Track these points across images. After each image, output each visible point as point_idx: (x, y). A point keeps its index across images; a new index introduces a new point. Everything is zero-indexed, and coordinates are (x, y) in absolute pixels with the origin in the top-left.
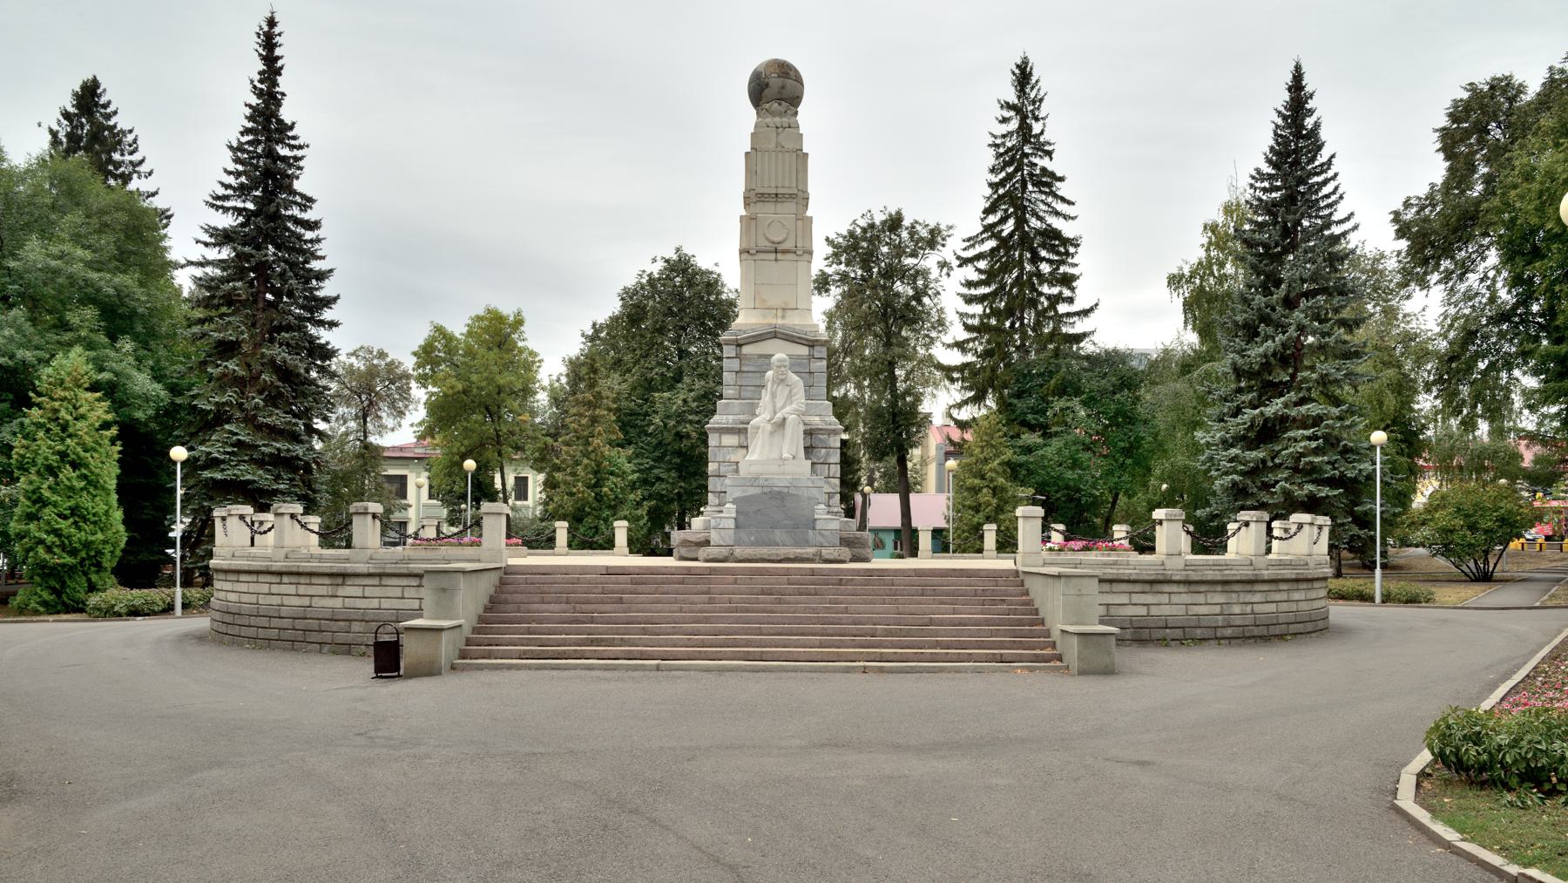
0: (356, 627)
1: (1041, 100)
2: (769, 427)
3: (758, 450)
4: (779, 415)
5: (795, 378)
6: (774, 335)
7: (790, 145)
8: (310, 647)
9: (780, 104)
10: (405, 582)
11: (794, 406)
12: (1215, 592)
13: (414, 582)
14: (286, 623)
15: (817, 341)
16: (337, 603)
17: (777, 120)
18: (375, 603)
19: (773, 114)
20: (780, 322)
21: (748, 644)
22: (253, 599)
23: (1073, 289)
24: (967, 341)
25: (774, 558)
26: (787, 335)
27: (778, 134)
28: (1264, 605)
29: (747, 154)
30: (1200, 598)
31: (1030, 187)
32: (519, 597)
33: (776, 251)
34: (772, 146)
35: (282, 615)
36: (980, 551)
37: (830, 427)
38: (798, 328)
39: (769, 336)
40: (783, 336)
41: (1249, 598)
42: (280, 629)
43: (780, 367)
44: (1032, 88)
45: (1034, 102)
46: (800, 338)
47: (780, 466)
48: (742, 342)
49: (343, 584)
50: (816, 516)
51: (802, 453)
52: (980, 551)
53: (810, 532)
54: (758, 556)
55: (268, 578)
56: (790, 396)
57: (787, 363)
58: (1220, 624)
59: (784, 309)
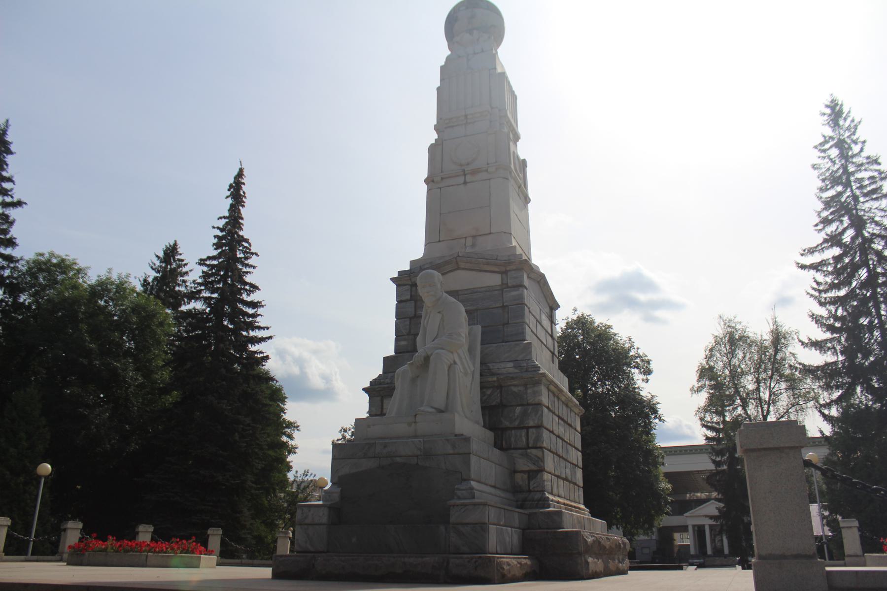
1: (856, 127)
23: (820, 180)
24: (826, 341)
31: (862, 199)
44: (845, 119)
45: (848, 129)
47: (409, 424)
53: (442, 528)
59: (474, 237)
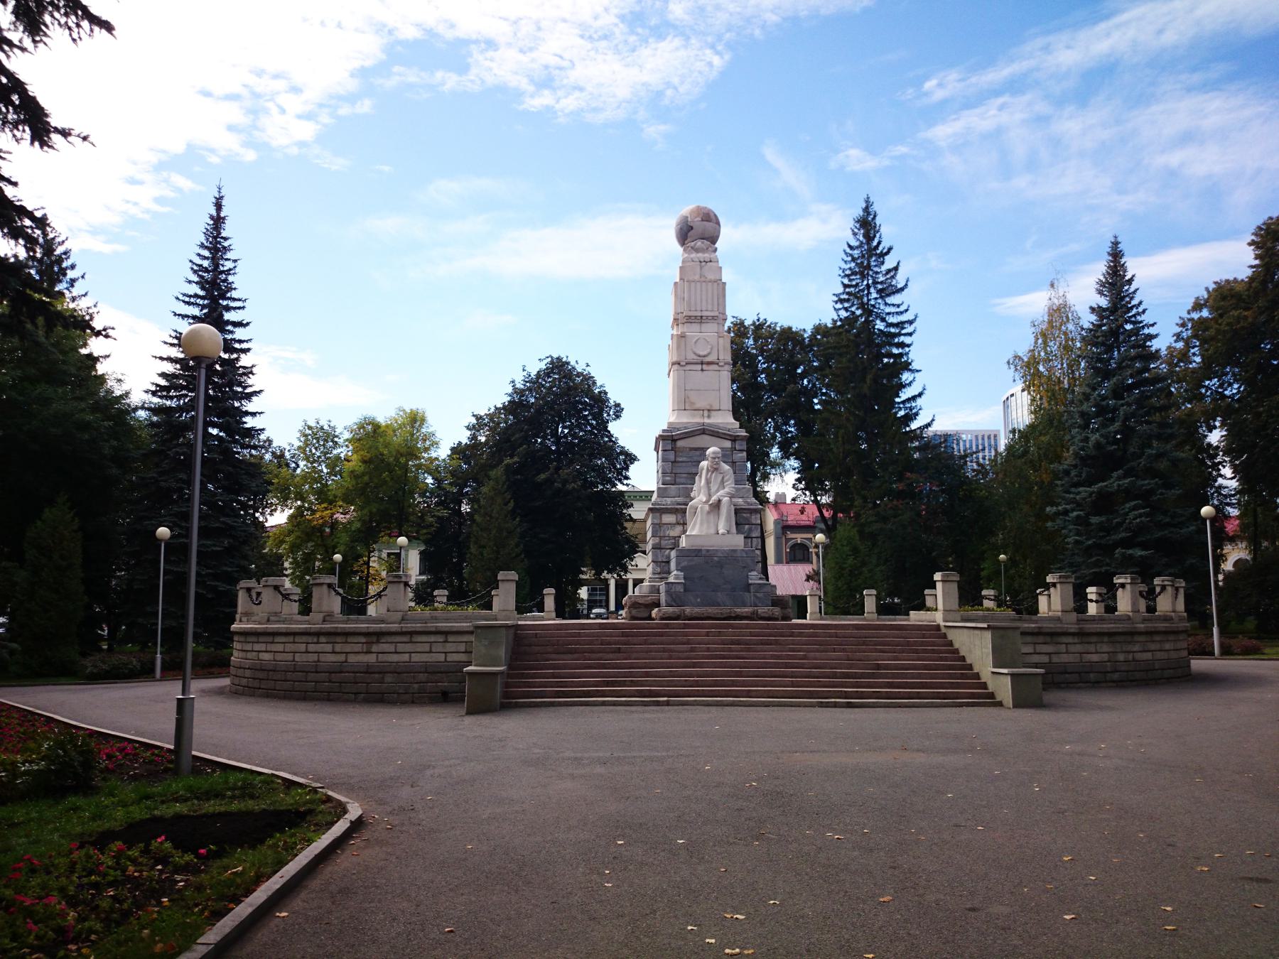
0: (389, 678)
2: (707, 507)
3: (698, 526)
4: (714, 498)
5: (726, 467)
6: (703, 431)
7: (711, 277)
8: (346, 696)
9: (703, 243)
10: (432, 638)
11: (727, 490)
12: (1103, 642)
13: (440, 638)
14: (323, 676)
15: (738, 436)
16: (371, 658)
17: (700, 255)
18: (406, 657)
19: (697, 250)
20: (707, 421)
21: (733, 684)
22: (290, 657)
25: (719, 616)
26: (713, 431)
27: (701, 268)
28: (1142, 653)
29: (676, 283)
30: (1092, 648)
32: (536, 649)
33: (702, 363)
34: (697, 277)
35: (1069, 671)
36: (541, 610)
37: (752, 507)
38: (721, 425)
39: (699, 432)
40: (711, 433)
41: (1130, 648)
42: (316, 682)
43: (714, 458)
46: (725, 434)
48: (675, 438)
49: (378, 642)
50: (750, 582)
51: (734, 529)
52: (541, 610)
54: (705, 615)
55: (304, 639)
56: (723, 482)
57: (720, 455)
58: (1109, 669)
59: (709, 410)
